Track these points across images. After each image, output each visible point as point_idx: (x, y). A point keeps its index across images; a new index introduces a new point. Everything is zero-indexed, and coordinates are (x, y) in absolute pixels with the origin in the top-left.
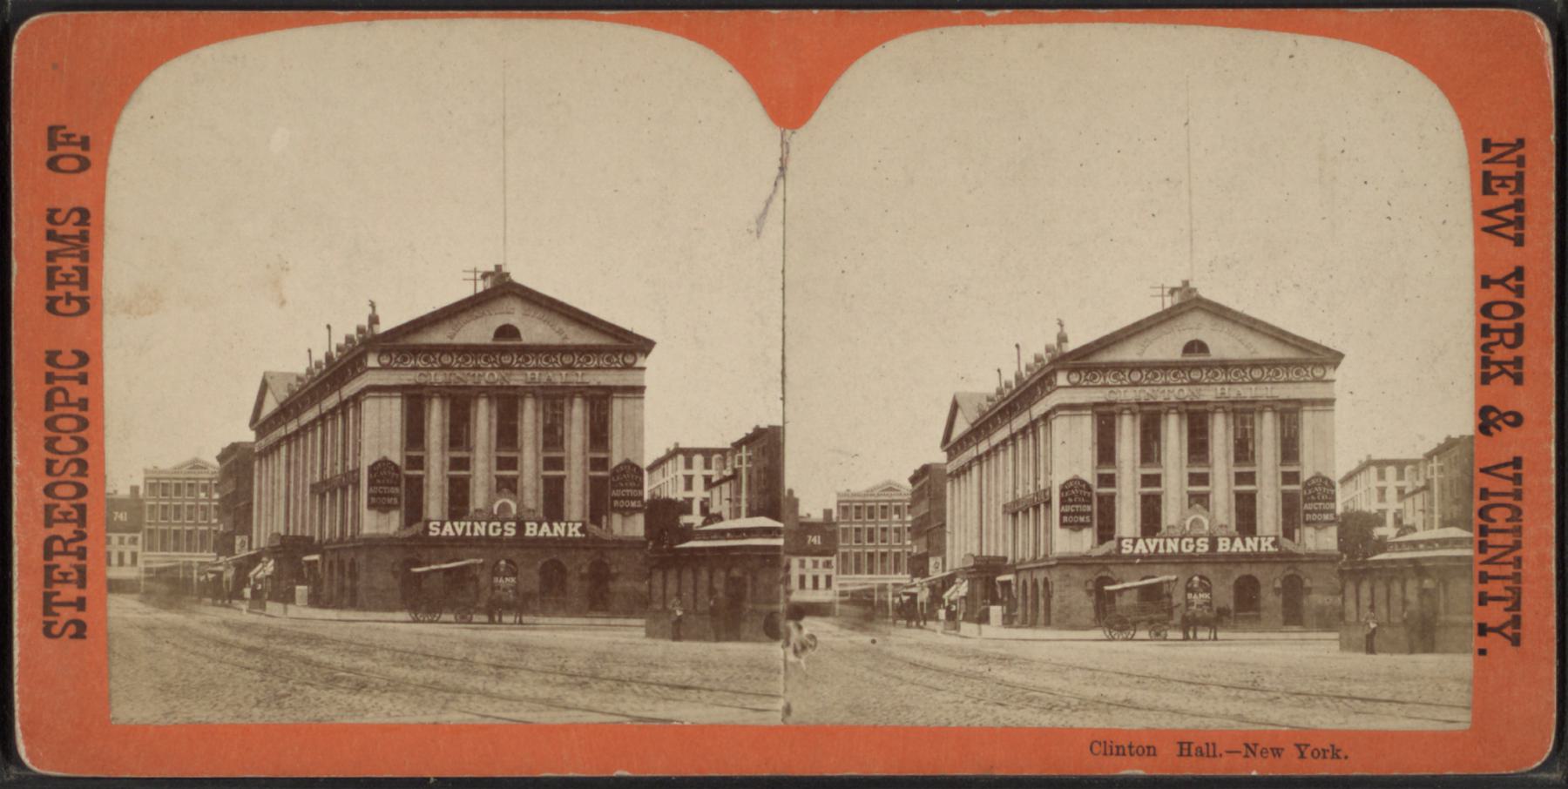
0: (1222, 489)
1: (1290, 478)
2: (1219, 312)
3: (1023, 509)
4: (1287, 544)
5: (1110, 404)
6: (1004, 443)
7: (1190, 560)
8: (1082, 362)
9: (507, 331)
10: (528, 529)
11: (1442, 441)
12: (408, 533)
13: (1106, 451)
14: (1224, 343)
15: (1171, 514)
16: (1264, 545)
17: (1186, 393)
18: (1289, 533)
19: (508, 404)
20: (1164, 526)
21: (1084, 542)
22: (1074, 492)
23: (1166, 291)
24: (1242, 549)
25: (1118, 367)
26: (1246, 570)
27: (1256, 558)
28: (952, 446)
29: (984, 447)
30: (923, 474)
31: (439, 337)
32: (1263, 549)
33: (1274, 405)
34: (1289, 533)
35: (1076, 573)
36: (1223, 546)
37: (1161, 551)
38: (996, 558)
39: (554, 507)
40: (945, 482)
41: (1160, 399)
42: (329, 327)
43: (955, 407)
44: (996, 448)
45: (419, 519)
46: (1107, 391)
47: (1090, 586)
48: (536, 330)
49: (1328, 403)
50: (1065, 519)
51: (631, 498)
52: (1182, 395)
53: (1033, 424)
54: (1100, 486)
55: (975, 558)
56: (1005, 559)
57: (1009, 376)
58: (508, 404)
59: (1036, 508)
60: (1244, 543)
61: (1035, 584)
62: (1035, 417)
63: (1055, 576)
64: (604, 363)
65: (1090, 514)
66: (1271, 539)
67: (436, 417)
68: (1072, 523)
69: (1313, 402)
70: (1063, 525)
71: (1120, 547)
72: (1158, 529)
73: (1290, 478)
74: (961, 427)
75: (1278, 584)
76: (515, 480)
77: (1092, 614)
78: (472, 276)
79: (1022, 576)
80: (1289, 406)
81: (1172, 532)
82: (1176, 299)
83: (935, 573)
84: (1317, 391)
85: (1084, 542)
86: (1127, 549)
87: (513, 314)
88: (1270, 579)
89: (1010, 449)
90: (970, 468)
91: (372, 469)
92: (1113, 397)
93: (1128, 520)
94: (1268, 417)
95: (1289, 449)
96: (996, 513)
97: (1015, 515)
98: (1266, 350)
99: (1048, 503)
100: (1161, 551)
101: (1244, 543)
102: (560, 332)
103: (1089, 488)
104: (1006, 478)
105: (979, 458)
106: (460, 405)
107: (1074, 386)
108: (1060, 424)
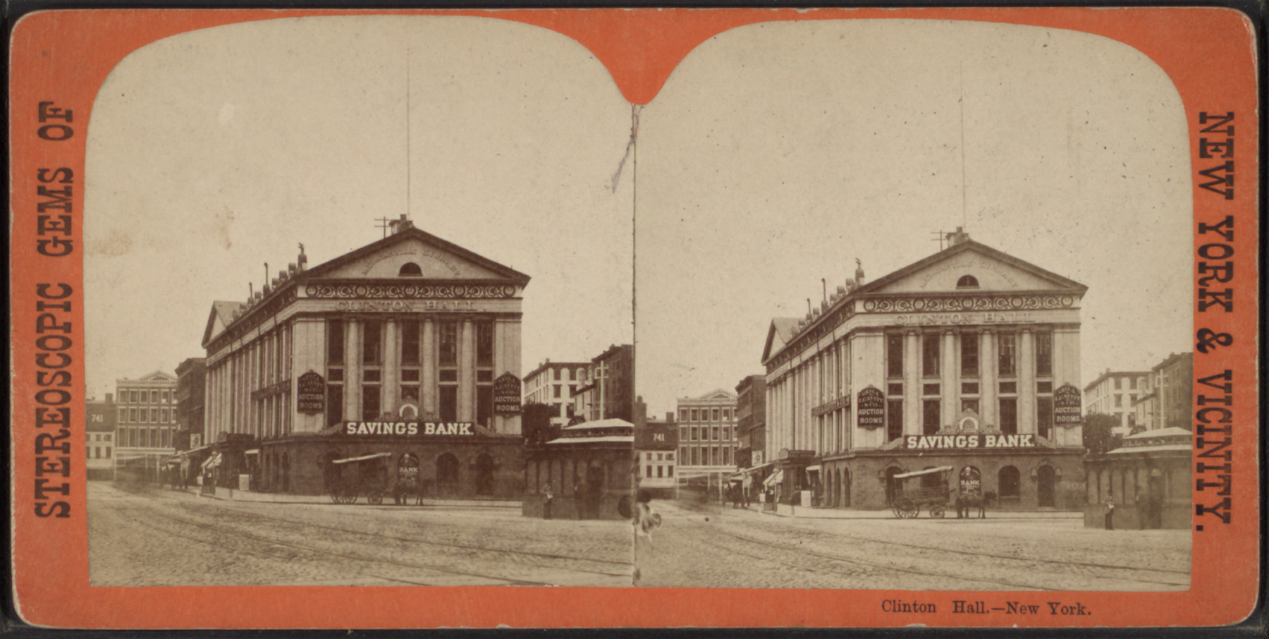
0: (989, 397)
1: (1044, 387)
2: (987, 253)
3: (828, 412)
4: (1041, 440)
5: (899, 327)
6: (813, 358)
7: (963, 454)
8: (875, 293)
9: (410, 268)
10: (428, 429)
11: (1167, 357)
12: (330, 432)
13: (895, 366)
14: (990, 278)
15: (948, 416)
16: (1023, 441)
17: (960, 318)
18: (1043, 432)
19: (411, 327)
20: (942, 426)
21: (877, 439)
22: (869, 398)
23: (944, 236)
24: (1005, 445)
25: (906, 297)
26: (1008, 462)
27: (1016, 452)
28: (771, 361)
29: (796, 362)
30: (747, 384)
31: (355, 273)
32: (1022, 445)
33: (1032, 328)
34: (1043, 432)
35: (871, 464)
36: (990, 442)
37: (940, 446)
38: (806, 452)
39: (448, 411)
40: (765, 390)
41: (939, 323)
42: (266, 265)
43: (773, 329)
44: (806, 363)
45: (339, 420)
46: (896, 316)
47: (882, 475)
48: (434, 267)
49: (1075, 326)
50: (862, 420)
51: (512, 404)
52: (956, 320)
53: (836, 343)
54: (890, 393)
55: (229, 436)
56: (813, 453)
57: (817, 305)
58: (411, 327)
59: (839, 411)
60: (1007, 440)
61: (838, 473)
62: (837, 337)
63: (854, 466)
64: (489, 294)
65: (882, 416)
66: (1029, 437)
67: (353, 337)
68: (867, 424)
69: (1063, 326)
70: (860, 425)
71: (906, 443)
72: (938, 428)
73: (1044, 387)
74: (778, 346)
75: (1034, 473)
76: (416, 388)
77: (884, 497)
78: (382, 223)
79: (827, 467)
80: (1043, 329)
81: (948, 431)
82: (952, 242)
83: (757, 464)
84: (1066, 317)
85: (877, 439)
86: (912, 444)
87: (415, 254)
88: (1028, 470)
89: (818, 364)
90: (785, 379)
91: (301, 380)
92: (900, 322)
93: (913, 421)
94: (1026, 338)
95: (1044, 364)
96: (806, 415)
97: (821, 417)
98: (1025, 283)
99: (848, 408)
100: (940, 446)
101: (1007, 440)
102: (453, 269)
103: (881, 395)
104: (814, 387)
105: (792, 371)
106: (372, 328)
107: (870, 312)
108: (858, 343)
